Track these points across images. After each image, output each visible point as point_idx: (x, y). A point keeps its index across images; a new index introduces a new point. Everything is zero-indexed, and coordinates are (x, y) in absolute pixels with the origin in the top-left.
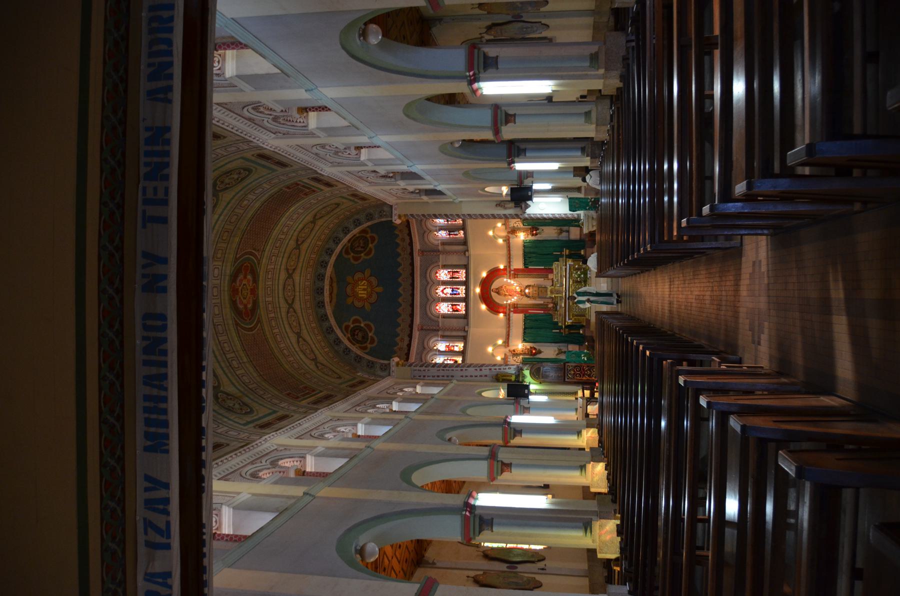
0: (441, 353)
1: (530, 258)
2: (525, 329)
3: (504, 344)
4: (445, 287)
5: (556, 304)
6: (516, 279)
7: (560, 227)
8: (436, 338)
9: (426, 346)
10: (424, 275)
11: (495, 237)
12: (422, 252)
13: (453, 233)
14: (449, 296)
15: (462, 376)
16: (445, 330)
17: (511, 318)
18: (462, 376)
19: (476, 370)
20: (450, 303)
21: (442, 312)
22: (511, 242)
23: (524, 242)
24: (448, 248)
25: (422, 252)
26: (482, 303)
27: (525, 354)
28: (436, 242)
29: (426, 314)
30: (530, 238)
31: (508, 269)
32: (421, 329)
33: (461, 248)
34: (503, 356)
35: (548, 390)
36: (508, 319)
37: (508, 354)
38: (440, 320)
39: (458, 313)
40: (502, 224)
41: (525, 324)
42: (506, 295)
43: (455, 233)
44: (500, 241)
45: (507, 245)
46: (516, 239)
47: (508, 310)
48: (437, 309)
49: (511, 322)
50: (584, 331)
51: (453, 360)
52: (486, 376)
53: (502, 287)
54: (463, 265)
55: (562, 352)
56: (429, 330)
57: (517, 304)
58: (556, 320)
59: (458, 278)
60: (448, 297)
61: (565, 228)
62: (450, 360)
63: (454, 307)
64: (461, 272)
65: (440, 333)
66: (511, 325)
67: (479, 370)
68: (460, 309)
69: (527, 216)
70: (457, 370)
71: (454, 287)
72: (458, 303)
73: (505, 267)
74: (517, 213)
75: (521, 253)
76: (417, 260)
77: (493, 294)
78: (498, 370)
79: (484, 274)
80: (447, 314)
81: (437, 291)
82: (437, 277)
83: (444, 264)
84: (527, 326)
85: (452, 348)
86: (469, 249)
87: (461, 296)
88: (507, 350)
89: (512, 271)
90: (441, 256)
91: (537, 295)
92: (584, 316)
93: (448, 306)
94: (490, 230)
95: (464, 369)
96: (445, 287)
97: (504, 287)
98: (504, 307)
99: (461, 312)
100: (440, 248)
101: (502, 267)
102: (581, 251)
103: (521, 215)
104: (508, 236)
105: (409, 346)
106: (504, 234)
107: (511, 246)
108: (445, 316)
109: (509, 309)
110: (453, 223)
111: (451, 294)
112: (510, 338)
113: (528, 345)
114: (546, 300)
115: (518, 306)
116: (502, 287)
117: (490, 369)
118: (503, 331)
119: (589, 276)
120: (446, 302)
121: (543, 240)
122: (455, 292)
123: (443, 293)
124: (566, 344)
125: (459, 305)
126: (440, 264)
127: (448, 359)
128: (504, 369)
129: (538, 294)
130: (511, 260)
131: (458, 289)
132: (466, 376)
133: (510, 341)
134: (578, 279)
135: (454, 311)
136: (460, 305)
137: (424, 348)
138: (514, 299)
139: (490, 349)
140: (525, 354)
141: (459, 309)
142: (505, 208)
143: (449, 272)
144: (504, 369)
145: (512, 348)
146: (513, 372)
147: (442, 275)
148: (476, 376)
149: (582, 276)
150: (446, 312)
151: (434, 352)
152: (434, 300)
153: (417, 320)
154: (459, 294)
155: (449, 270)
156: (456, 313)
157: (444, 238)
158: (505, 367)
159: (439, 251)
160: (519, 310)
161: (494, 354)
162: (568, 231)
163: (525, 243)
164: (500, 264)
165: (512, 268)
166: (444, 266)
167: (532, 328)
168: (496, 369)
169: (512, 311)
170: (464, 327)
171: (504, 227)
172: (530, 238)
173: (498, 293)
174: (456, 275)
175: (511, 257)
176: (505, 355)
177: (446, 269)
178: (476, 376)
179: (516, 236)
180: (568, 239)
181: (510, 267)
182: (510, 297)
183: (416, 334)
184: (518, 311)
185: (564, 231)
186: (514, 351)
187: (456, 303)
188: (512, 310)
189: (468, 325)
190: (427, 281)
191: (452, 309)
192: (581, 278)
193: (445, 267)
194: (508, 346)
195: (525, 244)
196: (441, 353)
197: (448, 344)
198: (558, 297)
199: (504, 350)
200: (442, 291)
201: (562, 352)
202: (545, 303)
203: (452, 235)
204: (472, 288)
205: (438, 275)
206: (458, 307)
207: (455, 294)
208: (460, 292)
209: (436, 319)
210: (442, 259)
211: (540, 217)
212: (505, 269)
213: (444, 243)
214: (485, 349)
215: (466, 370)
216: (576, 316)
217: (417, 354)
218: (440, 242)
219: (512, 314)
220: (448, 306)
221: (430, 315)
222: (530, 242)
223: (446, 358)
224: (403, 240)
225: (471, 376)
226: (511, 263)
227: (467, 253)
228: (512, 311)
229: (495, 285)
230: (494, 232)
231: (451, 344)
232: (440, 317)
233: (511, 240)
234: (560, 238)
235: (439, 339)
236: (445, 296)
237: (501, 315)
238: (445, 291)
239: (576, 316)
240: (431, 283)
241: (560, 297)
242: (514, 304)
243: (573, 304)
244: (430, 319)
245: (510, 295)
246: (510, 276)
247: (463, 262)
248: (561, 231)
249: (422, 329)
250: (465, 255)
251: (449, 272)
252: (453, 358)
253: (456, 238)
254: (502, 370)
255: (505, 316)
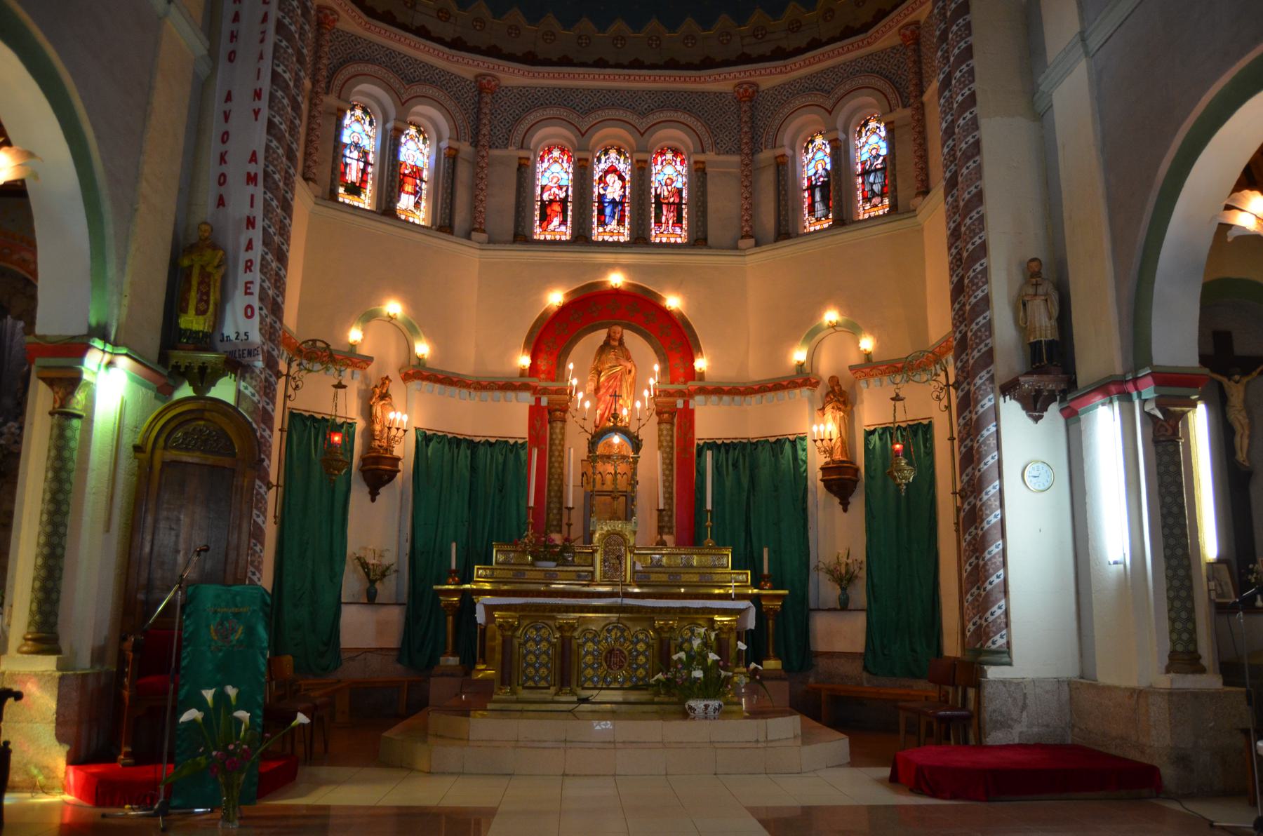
0: (391, 145)
1: (735, 465)
2: (472, 445)
3: (414, 362)
4: (628, 178)
5: (560, 555)
6: (655, 419)
7: (863, 574)
8: (446, 131)
9: (418, 89)
10: (668, 101)
11: (812, 334)
12: (749, 96)
13: (818, 197)
14: (597, 190)
15: (229, 98)
16: (477, 166)
17: (511, 395)
18: (229, 98)
19: (254, 158)
20: (570, 193)
21: (540, 167)
22: (797, 391)
23: (796, 443)
24: (767, 181)
25: (749, 96)
26: (567, 295)
27: (369, 434)
28: (786, 138)
29: (528, 110)
30: (816, 461)
31: (693, 385)
32: (483, 87)
33: (767, 219)
34: (364, 351)
35: (83, 492)
36: (508, 386)
37: (372, 369)
38: (513, 152)
39: (537, 218)
40: (868, 356)
41: (491, 444)
42: (599, 373)
43: (819, 207)
44: (799, 355)
45: (784, 378)
46: (806, 410)
47: (544, 384)
48: (550, 152)
49: (498, 394)
50: (449, 673)
51: (364, 181)
52: (221, 202)
53: (628, 358)
54: (705, 232)
55: (372, 582)
56: (478, 119)
57: (564, 421)
58: (497, 556)
59: (658, 222)
60: (592, 187)
61: (859, 594)
62: (364, 171)
63: (557, 208)
64: (678, 230)
65: (465, 148)
66: (485, 394)
67: (253, 168)
68: (551, 227)
69: (988, 403)
70: (261, 57)
71: (627, 209)
72: (569, 219)
73: (702, 374)
74: (998, 356)
75: (752, 431)
76: (720, 82)
77: (601, 335)
78: (244, 256)
79: (673, 302)
80: (534, 186)
81: (613, 154)
82: (662, 154)
83: (708, 170)
84: (481, 450)
85: (408, 188)
86: (764, 248)
87: (595, 232)
88: (393, 373)
89: (686, 403)
90: (735, 159)
91: (598, 487)
92: (506, 678)
93: (560, 188)
94: (841, 314)
95: (263, 104)
96: (628, 178)
97: (629, 365)
98: (557, 372)
99: (538, 230)
100: (766, 155)
101: (701, 364)
102: (777, 657)
103: (992, 379)
104: (817, 383)
105: (423, 32)
106: (825, 367)
107: (780, 394)
108: (525, 173)
109: (545, 391)
110: (859, 193)
111: (601, 197)
112: (437, 386)
113: (404, 449)
114: (576, 518)
115: (559, 424)
116: (628, 358)
117: (251, 223)
118: (466, 366)
119: (698, 704)
120: (574, 180)
121: (805, 510)
122: (608, 211)
123: (607, 172)
124: (404, 598)
125: (563, 222)
126: (710, 156)
127: (367, 163)
128: (248, 285)
129: (602, 493)
130: (726, 398)
131: (621, 222)
132: (227, 117)
133: (426, 385)
134: (682, 655)
135: (544, 207)
136: (563, 228)
137: (411, 81)
138: (583, 402)
139: (394, 307)
140: (369, 434)
141: (550, 222)
142: (1021, 305)
143: (680, 191)
144: (248, 285)
145: (397, 389)
146: (229, 330)
147: (669, 170)
148: (223, 159)
149: (698, 674)
150: (542, 180)
151: (392, 113)
152: (583, 135)
153: (513, 77)
154: (602, 223)
155: (684, 194)
156: (537, 213)
157: (799, 169)
158: (256, 289)
159: (754, 152)
160: (543, 425)
161: (374, 323)
162: (844, 606)
163: (793, 443)
164: (711, 360)
165: (697, 403)
166: (703, 171)
167: (473, 469)
168: (249, 247)
169: (538, 400)
170: (484, 231)
171: (855, 359)
172: (816, 461)
173: (606, 347)
174: (668, 216)
175: (737, 398)
176: (368, 360)
177: (690, 184)
178: (223, 159)
179: (823, 409)
180: (812, 606)
181: (704, 391)
182: (591, 386)
183: (466, 67)
184: (538, 424)
185: (843, 589)
186: (385, 396)
187: (570, 213)
188: (544, 401)
189: (490, 241)
190: (651, 111)
191: (551, 201)
192: (688, 665)
193: (699, 175)
194: (407, 377)
195: (788, 447)
196: (391, 145)
197: (425, 175)
198: (592, 565)
199: (389, 358)
200: (612, 170)
201: (372, 582)
202: (565, 512)
203: (812, 196)
204: (626, 258)
205: (669, 156)
206: (556, 221)
207: (601, 212)
208: (608, 228)
209: (517, 138)
210: (725, 164)
211: (984, 467)
212: (691, 374)
213: (784, 169)
214: (396, 289)
215: (256, 113)
216: (506, 642)
217: (391, 53)
218: (789, 152)
219: (527, 399)
220: (560, 188)
221: (532, 118)
222: (798, 464)
223: (371, 158)
224: (795, 27)
225: (225, 137)
226: (714, 398)
227: (752, 241)
228: (538, 400)
229: (633, 341)
230: (834, 326)
231: (424, 186)
232: (523, 153)
233: (805, 391)
234: (813, 576)
235: (444, 144)
236: (596, 177)
237: (524, 361)
238: (611, 178)
239: (506, 642)
240: (643, 124)
241: (593, 573)
242: (565, 410)
243: (560, 628)
244: (517, 120)
245: (597, 390)
246: (668, 394)
247: (713, 233)
248: (844, 579)
249: (481, 90)
250: (743, 237)
251: (680, 191)
252: (370, 182)
253: (802, 209)
254: (243, 277)
255: (522, 373)
